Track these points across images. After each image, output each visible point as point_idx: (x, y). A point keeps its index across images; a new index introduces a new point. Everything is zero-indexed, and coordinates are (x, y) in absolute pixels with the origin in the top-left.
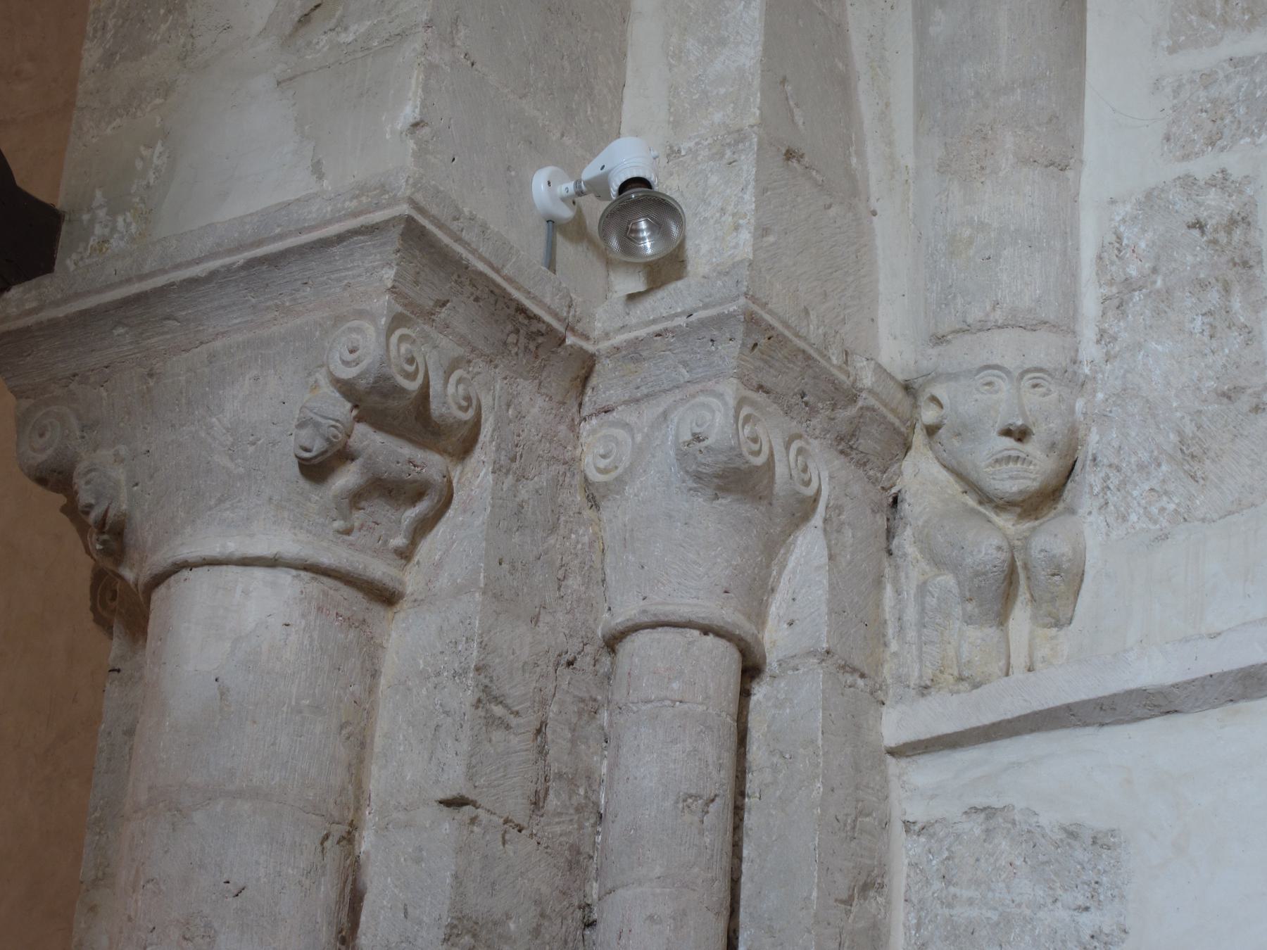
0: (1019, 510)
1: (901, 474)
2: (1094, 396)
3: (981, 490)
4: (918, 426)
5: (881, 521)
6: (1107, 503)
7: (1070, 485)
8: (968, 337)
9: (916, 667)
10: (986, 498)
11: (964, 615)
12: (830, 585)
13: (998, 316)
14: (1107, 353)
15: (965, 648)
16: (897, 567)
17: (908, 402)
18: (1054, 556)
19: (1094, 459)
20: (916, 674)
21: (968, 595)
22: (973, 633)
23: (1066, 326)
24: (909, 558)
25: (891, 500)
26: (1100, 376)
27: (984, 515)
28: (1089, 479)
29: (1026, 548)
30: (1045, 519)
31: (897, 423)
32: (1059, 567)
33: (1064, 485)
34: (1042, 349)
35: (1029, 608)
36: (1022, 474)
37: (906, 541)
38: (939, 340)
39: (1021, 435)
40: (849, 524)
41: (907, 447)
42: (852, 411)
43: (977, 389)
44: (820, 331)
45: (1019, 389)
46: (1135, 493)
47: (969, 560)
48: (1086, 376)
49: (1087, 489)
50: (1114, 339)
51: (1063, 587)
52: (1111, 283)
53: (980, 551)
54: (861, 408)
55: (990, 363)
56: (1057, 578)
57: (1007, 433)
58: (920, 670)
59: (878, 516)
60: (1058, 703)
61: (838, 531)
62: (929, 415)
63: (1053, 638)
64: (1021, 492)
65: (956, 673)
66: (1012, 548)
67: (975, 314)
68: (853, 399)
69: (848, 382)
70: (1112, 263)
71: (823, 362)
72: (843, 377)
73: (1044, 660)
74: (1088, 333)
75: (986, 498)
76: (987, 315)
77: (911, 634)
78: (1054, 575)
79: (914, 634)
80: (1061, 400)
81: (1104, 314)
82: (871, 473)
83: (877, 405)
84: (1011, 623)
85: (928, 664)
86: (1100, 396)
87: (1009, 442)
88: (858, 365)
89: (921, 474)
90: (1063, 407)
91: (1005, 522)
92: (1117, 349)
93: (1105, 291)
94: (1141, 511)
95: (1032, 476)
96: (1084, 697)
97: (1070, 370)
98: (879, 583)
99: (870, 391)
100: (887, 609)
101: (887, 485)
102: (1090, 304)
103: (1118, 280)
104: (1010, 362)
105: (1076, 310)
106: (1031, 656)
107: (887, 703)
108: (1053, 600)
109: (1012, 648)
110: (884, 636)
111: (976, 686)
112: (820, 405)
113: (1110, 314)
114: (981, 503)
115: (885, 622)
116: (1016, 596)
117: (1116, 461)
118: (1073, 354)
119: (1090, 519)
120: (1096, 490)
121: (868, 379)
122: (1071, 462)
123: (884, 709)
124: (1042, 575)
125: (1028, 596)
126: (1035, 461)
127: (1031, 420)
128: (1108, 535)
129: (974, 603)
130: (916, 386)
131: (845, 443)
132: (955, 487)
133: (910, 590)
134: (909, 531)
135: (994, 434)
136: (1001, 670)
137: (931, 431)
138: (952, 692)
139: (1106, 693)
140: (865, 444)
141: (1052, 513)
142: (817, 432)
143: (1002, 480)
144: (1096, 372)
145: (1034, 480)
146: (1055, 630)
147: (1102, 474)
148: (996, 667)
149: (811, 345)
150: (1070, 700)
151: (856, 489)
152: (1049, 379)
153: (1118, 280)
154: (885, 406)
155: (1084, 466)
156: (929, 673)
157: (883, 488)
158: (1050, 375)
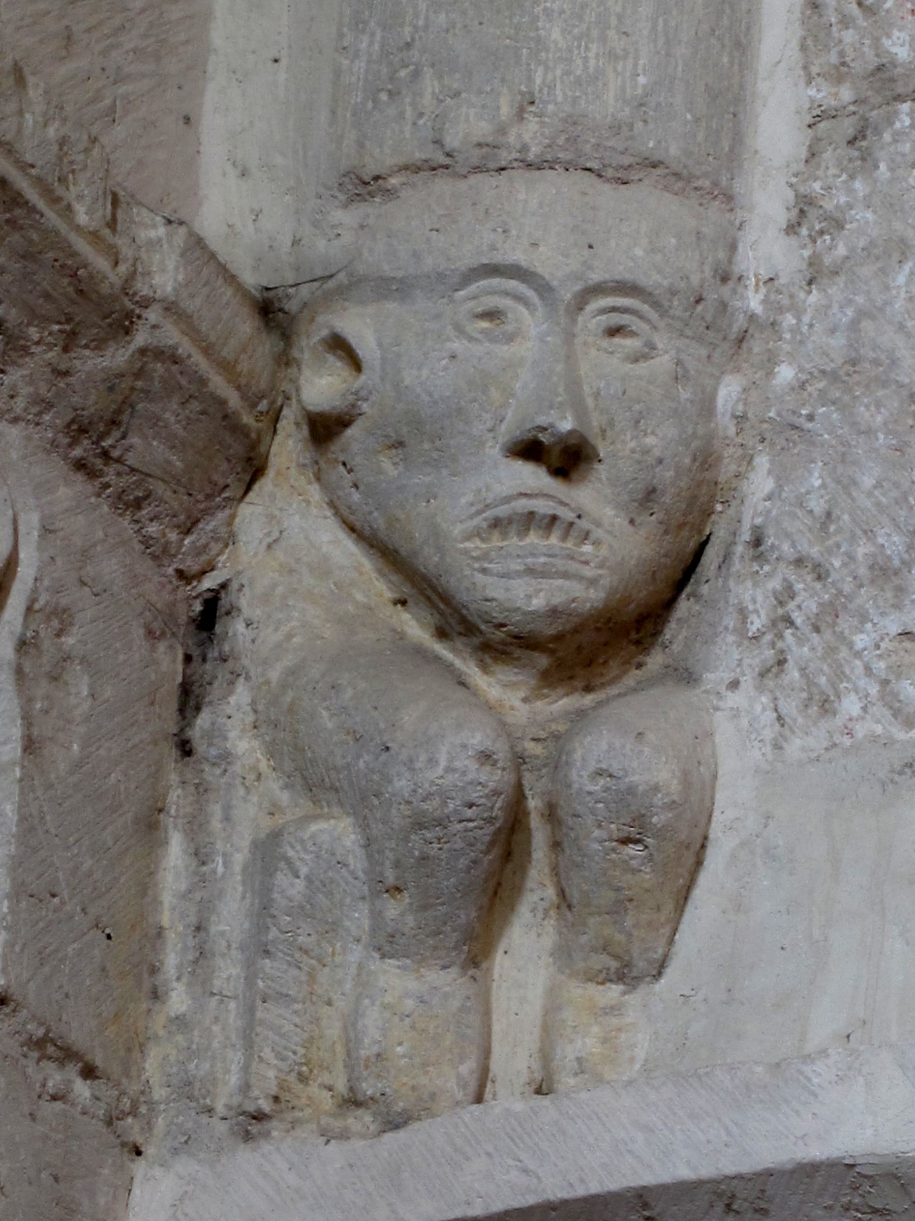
0: (543, 661)
1: (230, 539)
2: (770, 374)
3: (446, 598)
4: (289, 416)
5: (169, 662)
6: (781, 662)
7: (684, 606)
8: (443, 185)
9: (236, 1058)
10: (457, 621)
11: (374, 930)
12: (23, 819)
13: (531, 135)
14: (814, 262)
15: (372, 1021)
16: (202, 789)
17: (266, 347)
18: (631, 790)
19: (757, 542)
20: (234, 1079)
21: (390, 877)
22: (395, 980)
23: (708, 179)
24: (237, 768)
25: (198, 607)
26: (789, 320)
27: (449, 668)
28: (739, 594)
29: (557, 764)
30: (613, 691)
31: (234, 400)
32: (640, 820)
33: (669, 604)
34: (640, 235)
35: (550, 925)
36: (560, 564)
37: (233, 722)
38: (365, 186)
39: (566, 458)
40: (83, 660)
41: (254, 469)
42: (117, 357)
43: (460, 330)
44: (52, 132)
45: (569, 337)
46: (861, 641)
47: (402, 784)
48: (752, 317)
49: (731, 621)
50: (836, 223)
51: (647, 876)
52: (839, 73)
53: (432, 761)
54: (143, 351)
55: (497, 258)
56: (632, 850)
57: (530, 450)
58: (246, 1069)
59: (162, 647)
60: (613, 1184)
61: (55, 678)
62: (321, 386)
63: (613, 1010)
64: (554, 612)
65: (341, 1086)
66: (520, 760)
67: (469, 126)
68: (123, 325)
69: (114, 277)
70: (846, 22)
71: (52, 218)
72: (101, 263)
73: (581, 1066)
74: (767, 202)
75: (457, 621)
76: (502, 130)
77: (228, 971)
78: (626, 841)
79: (236, 971)
80: (680, 375)
81: (812, 154)
82: (153, 529)
83: (185, 347)
84: (501, 964)
85: (267, 1054)
86: (786, 373)
87: (532, 476)
88: (145, 234)
89: (286, 546)
90: (685, 394)
91: (506, 691)
92: (841, 250)
93: (821, 93)
94: (874, 690)
95: (588, 572)
96: (685, 1173)
97: (711, 297)
98: (150, 825)
99: (171, 308)
100: (167, 899)
101: (192, 565)
102: (777, 127)
103: (857, 67)
104: (552, 259)
105: (738, 138)
106: (546, 1056)
107: (150, 1151)
108: (618, 908)
109: (496, 1028)
110: (154, 971)
111: (394, 1123)
112: (34, 333)
113: (828, 155)
114: (442, 634)
115: (160, 932)
116: (517, 890)
117: (815, 552)
118: (721, 255)
119: (733, 699)
120: (756, 624)
121: (165, 276)
122: (693, 544)
123: (139, 1167)
124: (595, 838)
125: (551, 892)
126: (598, 533)
127: (596, 421)
128: (777, 747)
129: (406, 898)
130: (292, 306)
131: (91, 441)
132: (374, 586)
133: (234, 853)
134: (241, 695)
135: (494, 451)
136: (464, 1086)
137: (325, 429)
138: (328, 1136)
139: (745, 1168)
140: (143, 448)
141: (632, 677)
142: (20, 404)
143: (505, 576)
144: (781, 310)
145: (593, 582)
146: (615, 990)
147: (775, 584)
148: (452, 1078)
149: (25, 167)
150: (647, 1179)
151: (110, 568)
152: (653, 315)
153: (857, 67)
154: (207, 350)
155: (727, 558)
156: (268, 1077)
157: (180, 574)
158: (656, 304)
